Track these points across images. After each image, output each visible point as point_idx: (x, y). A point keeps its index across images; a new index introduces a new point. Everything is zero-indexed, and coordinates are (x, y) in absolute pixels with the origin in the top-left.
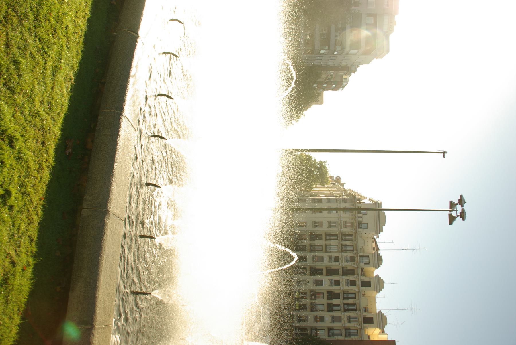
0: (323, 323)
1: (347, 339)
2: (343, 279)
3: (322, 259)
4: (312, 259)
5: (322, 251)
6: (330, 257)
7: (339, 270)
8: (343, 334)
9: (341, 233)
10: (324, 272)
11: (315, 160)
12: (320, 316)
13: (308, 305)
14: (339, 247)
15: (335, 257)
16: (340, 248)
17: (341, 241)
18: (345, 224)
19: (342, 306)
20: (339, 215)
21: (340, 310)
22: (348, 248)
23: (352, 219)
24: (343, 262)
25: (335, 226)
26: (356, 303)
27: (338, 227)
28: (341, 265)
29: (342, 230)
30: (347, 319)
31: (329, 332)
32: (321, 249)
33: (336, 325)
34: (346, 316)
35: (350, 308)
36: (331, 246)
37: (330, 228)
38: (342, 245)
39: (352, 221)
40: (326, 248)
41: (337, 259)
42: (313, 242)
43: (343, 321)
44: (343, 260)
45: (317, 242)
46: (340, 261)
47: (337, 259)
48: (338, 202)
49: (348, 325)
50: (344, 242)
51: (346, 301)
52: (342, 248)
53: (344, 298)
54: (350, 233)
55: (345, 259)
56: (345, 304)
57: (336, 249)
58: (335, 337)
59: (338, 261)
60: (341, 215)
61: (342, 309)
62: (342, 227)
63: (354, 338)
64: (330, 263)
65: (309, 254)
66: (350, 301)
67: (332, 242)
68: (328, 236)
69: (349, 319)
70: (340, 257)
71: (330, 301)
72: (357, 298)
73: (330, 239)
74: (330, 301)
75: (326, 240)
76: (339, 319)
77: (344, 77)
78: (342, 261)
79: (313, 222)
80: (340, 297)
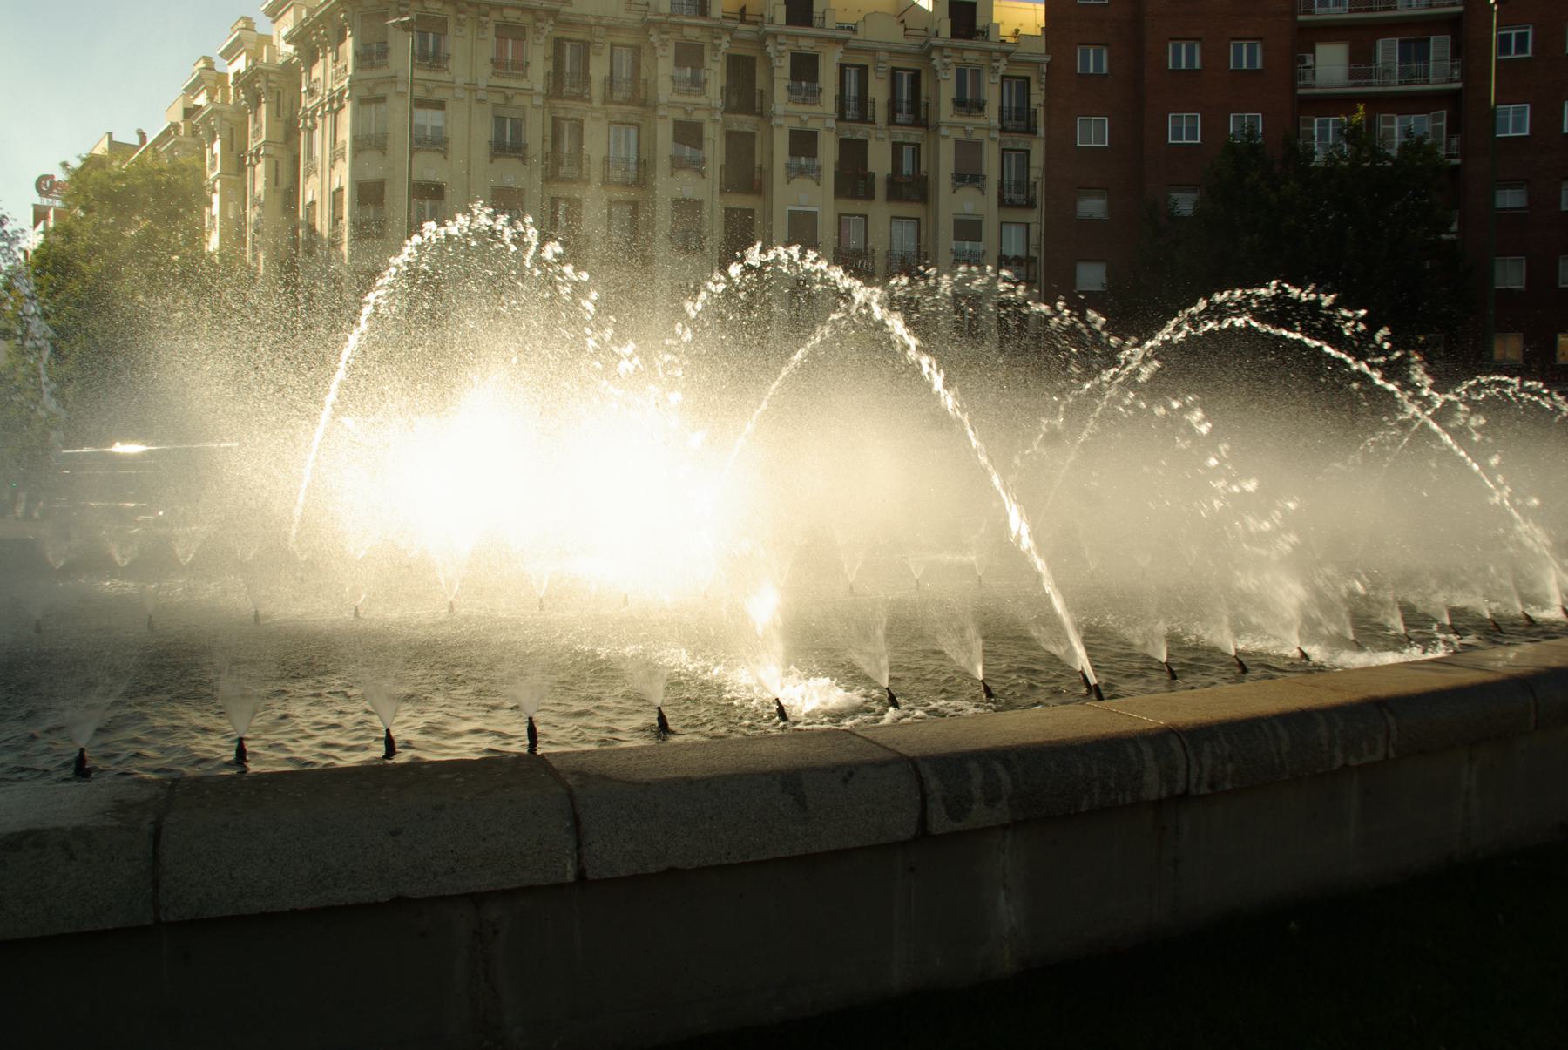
0: (984, 225)
1: (1041, 131)
2: (787, 115)
12: (955, 240)
19: (901, 134)
20: (459, 94)
23: (483, 26)
25: (518, 126)
26: (888, 66)
27: (522, 108)
30: (969, 113)
33: (991, 165)
34: (956, 119)
35: (905, 98)
39: (492, 26)
46: (698, 116)
48: (380, 92)
49: (992, 114)
53: (864, 117)
55: (689, 92)
56: (892, 121)
57: (627, 134)
58: (1032, 179)
60: (460, 81)
61: (914, 134)
62: (524, 84)
63: (1037, 97)
66: (878, 91)
70: (795, 124)
71: (880, 189)
72: (864, 60)
74: (880, 189)
76: (968, 150)
77: (106, 154)
78: (697, 107)
80: (859, 136)
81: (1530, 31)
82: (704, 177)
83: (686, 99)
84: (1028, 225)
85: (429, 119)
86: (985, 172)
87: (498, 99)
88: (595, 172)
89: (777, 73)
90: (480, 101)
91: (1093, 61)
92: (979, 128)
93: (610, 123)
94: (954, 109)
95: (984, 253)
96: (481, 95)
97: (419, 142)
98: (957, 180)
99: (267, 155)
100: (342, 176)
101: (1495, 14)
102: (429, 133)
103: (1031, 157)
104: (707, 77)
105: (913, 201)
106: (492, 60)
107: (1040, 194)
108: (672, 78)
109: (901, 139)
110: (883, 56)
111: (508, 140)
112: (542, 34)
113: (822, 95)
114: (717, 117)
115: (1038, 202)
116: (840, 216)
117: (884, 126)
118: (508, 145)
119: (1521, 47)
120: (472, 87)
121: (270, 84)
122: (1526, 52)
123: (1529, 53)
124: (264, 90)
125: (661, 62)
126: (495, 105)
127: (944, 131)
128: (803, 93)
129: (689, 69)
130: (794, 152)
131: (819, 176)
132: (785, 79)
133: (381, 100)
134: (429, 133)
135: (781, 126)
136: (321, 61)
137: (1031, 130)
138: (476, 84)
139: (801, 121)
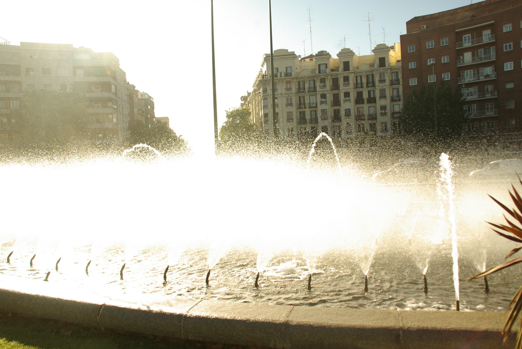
1: (401, 83)
2: (343, 89)
3: (323, 111)
6: (322, 103)
8: (397, 86)
9: (297, 93)
10: (336, 108)
11: (226, 123)
19: (369, 89)
22: (312, 85)
23: (283, 83)
24: (326, 89)
25: (291, 99)
27: (292, 96)
29: (294, 92)
31: (396, 101)
33: (388, 94)
35: (371, 81)
36: (311, 102)
37: (293, 104)
38: (309, 92)
39: (285, 82)
41: (323, 96)
43: (384, 87)
44: (324, 89)
46: (325, 93)
47: (323, 96)
48: (266, 97)
49: (388, 82)
50: (307, 90)
52: (312, 91)
53: (362, 87)
54: (297, 84)
55: (323, 88)
56: (367, 86)
58: (400, 94)
59: (325, 95)
60: (280, 93)
61: (372, 88)
62: (291, 92)
63: (400, 76)
64: (328, 102)
66: (364, 81)
67: (307, 101)
68: (301, 106)
70: (321, 93)
71: (366, 101)
72: (361, 74)
73: (304, 104)
74: (366, 101)
76: (383, 91)
78: (325, 91)
80: (361, 91)
81: (512, 43)
83: (323, 90)
87: (287, 95)
91: (412, 65)
92: (384, 86)
93: (310, 96)
96: (284, 95)
98: (381, 97)
108: (320, 86)
110: (364, 73)
119: (506, 46)
122: (511, 49)
123: (512, 49)
126: (286, 97)
127: (377, 88)
130: (345, 96)
135: (342, 92)
137: (399, 84)
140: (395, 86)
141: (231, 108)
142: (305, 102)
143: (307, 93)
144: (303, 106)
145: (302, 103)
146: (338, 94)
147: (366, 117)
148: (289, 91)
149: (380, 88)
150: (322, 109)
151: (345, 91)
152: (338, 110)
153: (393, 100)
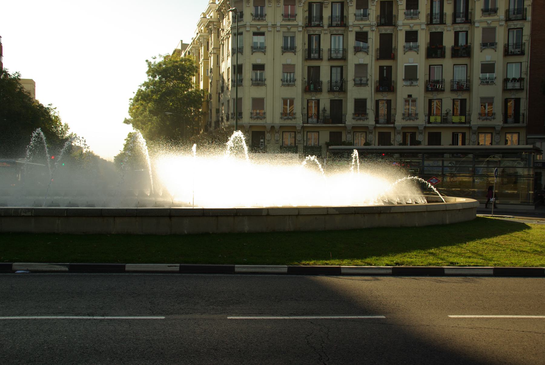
1: (529, 18)
2: (404, 25)
3: (361, 68)
4: (362, 88)
5: (342, 67)
6: (357, 50)
7: (383, 32)
8: (518, 24)
9: (306, 27)
10: (386, 63)
11: (146, 84)
12: (482, 73)
13: (455, 96)
14: (335, 32)
15: (356, 40)
16: (338, 31)
17: (323, 27)
18: (289, 16)
19: (458, 27)
20: (270, 29)
21: (467, 32)
22: (337, 13)
24: (367, 22)
25: (293, 38)
27: (295, 32)
28: (374, 28)
29: (300, 24)
30: (489, 15)
31: (513, 54)
32: (339, 69)
33: (501, 38)
34: (483, 18)
35: (462, 11)
36: (333, 47)
37: (298, 50)
38: (330, 26)
40: (337, 59)
41: (362, 36)
42: (325, 87)
43: (493, 25)
44: (363, 22)
45: (325, 77)
46: (365, 29)
47: (362, 36)
48: (240, 31)
49: (501, 14)
50: (326, 22)
51: (449, 19)
52: (337, 26)
53: (442, 22)
54: (306, 8)
55: (362, 20)
56: (454, 22)
58: (523, 41)
59: (366, 34)
60: (270, 24)
61: (465, 27)
64: (370, 49)
65: (349, 94)
67: (325, 45)
68: (312, 55)
69: (360, 83)
70: (358, 29)
71: (448, 53)
73: (319, 50)
74: (448, 53)
75: (320, 58)
78: (365, 25)
79: (283, 85)
80: (439, 30)
82: (368, 54)
84: (521, 63)
85: (259, 39)
86: (497, 41)
87: (285, 29)
88: (47, 154)
89: (400, 7)
90: (278, 31)
93: (331, 35)
94: (482, 14)
95: (495, 78)
96: (278, 29)
97: (255, 49)
99: (214, 53)
100: (229, 65)
101: (385, 71)
102: (259, 45)
103: (523, 31)
104: (370, 13)
105: (464, 57)
106: (282, 15)
107: (527, 49)
108: (355, 15)
109: (458, 30)
111: (289, 46)
112: (302, 2)
113: (420, 15)
114: (374, 29)
115: (526, 52)
116: (430, 66)
117: (450, 25)
118: (289, 47)
120: (275, 26)
121: (215, 26)
124: (213, 29)
125: (350, 8)
126: (284, 32)
127: (477, 24)
128: (412, 15)
129: (362, 10)
130: (407, 40)
131: (418, 50)
132: (404, 9)
133: (241, 34)
134: (259, 45)
135: (401, 30)
136: (225, 19)
137: (524, 19)
138: (276, 25)
139: (410, 27)
140: (516, 22)
141: (158, 57)
142: (321, 47)
143: (326, 27)
144: (314, 55)
145: (314, 48)
146: (391, 35)
147: (447, 87)
148: (289, 20)
149: (485, 25)
150: (357, 63)
151: (408, 28)
152: (389, 68)
153: (507, 53)
